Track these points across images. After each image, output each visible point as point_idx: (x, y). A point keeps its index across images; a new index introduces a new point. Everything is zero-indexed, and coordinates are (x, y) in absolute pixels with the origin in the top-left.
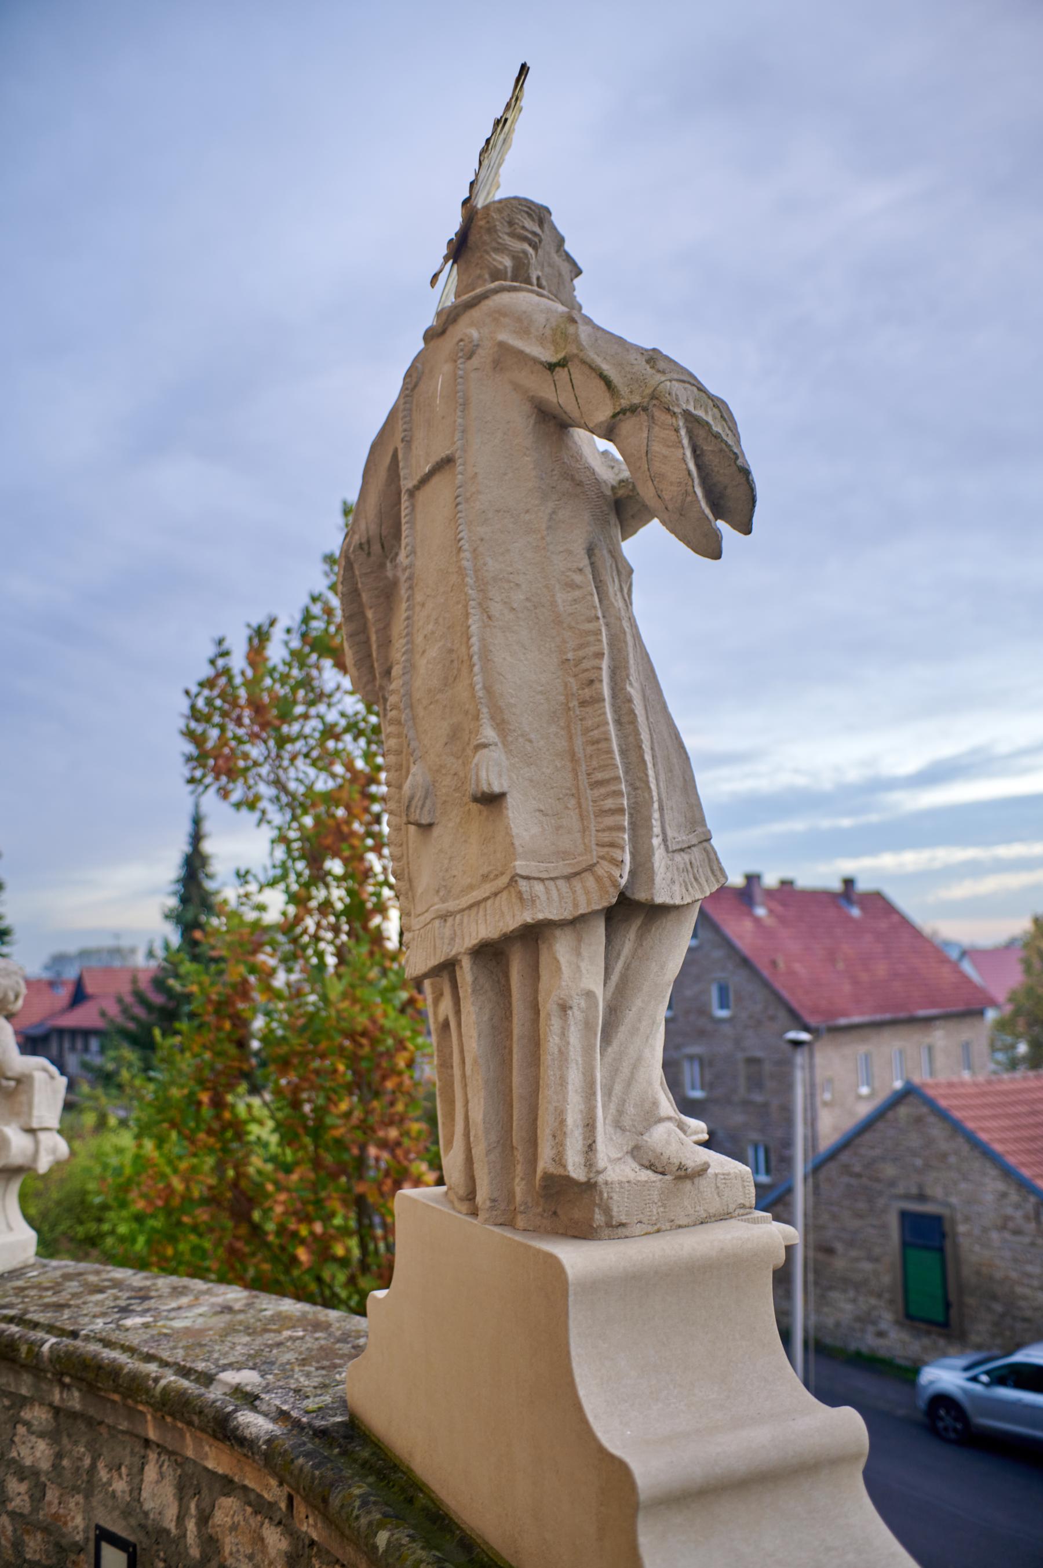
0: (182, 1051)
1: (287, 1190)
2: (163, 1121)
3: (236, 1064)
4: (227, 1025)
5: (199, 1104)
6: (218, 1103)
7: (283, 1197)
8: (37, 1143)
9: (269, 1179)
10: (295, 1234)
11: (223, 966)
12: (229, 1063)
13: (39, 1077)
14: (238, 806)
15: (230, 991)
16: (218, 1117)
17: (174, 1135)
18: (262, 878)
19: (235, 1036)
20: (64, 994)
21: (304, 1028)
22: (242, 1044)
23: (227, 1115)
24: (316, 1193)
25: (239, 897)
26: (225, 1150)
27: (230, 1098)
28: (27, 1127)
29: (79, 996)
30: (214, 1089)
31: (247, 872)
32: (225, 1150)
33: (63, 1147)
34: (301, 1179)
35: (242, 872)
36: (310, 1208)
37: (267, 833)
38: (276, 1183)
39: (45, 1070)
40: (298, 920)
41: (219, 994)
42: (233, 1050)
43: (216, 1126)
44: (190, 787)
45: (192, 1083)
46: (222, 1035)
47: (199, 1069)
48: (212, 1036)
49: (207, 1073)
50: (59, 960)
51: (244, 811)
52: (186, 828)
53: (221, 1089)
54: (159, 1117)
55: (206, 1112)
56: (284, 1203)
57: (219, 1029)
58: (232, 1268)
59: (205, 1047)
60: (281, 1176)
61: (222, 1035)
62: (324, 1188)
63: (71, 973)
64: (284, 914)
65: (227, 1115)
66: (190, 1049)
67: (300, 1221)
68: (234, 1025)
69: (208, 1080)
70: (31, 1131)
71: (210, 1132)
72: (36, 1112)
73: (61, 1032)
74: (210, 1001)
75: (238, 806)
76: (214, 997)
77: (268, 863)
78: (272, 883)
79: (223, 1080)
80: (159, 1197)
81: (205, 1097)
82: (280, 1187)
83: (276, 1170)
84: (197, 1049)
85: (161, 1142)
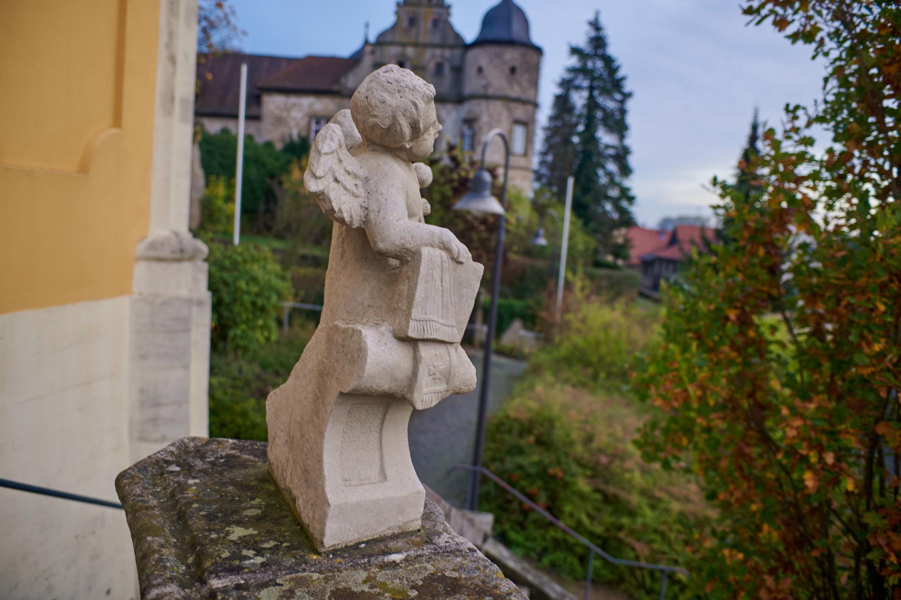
0: (716, 270)
1: (802, 416)
2: (689, 331)
3: (766, 289)
4: (762, 252)
5: (727, 319)
6: (744, 322)
7: (798, 423)
8: (416, 361)
9: (784, 403)
10: (804, 459)
11: (760, 131)
12: (759, 287)
13: (430, 256)
14: (794, 37)
15: (767, 220)
16: (743, 333)
17: (694, 345)
18: (812, 112)
19: (768, 263)
20: (665, 239)
21: (844, 261)
22: (774, 271)
23: (752, 334)
24: (832, 425)
25: (786, 132)
26: (746, 364)
27: (755, 319)
28: (403, 335)
29: (674, 240)
30: (742, 308)
31: (797, 107)
32: (746, 364)
33: (467, 372)
34: (819, 408)
35: (791, 107)
36: (824, 439)
37: (823, 66)
38: (792, 408)
39: (447, 249)
40: (846, 156)
41: (756, 221)
42: (764, 275)
43: (739, 341)
44: (748, 18)
45: (719, 300)
46: (756, 261)
47: (730, 289)
48: (745, 260)
49: (737, 292)
50: (666, 221)
51: (800, 43)
52: (747, 131)
53: (747, 309)
54: (685, 326)
55: (731, 329)
56: (797, 428)
57: (753, 254)
58: (740, 468)
59: (738, 270)
60: (798, 402)
61: (756, 261)
62: (842, 421)
63: (670, 228)
64: (830, 151)
65: (752, 334)
66: (724, 269)
67: (811, 448)
68: (768, 253)
69: (738, 300)
70: (412, 342)
71: (733, 346)
72: (416, 313)
73: (661, 260)
74: (747, 226)
75: (794, 37)
76: (752, 224)
77: (820, 99)
78: (820, 119)
79: (752, 302)
80: (676, 400)
81: (733, 315)
82: (795, 413)
83: (793, 395)
84: (730, 270)
85: (685, 349)
